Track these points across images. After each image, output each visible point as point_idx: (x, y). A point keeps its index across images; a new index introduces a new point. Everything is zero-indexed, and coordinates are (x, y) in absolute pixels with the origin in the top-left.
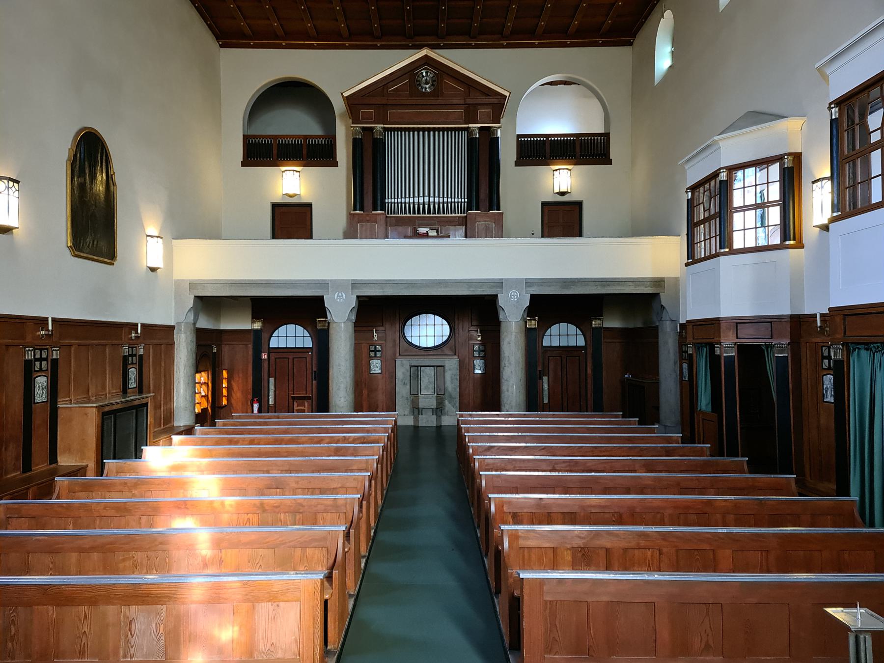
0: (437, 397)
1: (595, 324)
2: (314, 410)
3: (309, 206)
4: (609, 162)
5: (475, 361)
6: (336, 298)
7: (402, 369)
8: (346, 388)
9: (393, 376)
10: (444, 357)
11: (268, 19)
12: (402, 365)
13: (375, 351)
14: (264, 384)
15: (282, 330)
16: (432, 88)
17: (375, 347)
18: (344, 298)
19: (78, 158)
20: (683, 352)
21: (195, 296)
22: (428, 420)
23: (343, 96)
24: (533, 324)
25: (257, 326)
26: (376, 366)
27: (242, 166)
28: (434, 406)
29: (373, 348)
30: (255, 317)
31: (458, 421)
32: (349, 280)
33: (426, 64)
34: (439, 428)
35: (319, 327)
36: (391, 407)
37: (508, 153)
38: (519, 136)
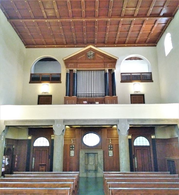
0: (95, 165)
1: (153, 137)
2: (49, 171)
4: (153, 81)
5: (109, 151)
6: (57, 126)
7: (82, 154)
8: (60, 162)
9: (78, 157)
10: (97, 149)
12: (82, 153)
13: (72, 147)
14: (31, 160)
15: (138, 138)
16: (93, 57)
17: (72, 146)
18: (60, 126)
20: (112, 147)
21: (6, 126)
22: (91, 175)
23: (63, 60)
24: (130, 137)
25: (30, 138)
26: (72, 153)
27: (121, 82)
28: (94, 169)
29: (71, 146)
30: (30, 134)
31: (104, 176)
32: (62, 119)
33: (91, 50)
34: (96, 178)
35: (52, 138)
36: (78, 170)
37: (118, 79)
38: (121, 73)
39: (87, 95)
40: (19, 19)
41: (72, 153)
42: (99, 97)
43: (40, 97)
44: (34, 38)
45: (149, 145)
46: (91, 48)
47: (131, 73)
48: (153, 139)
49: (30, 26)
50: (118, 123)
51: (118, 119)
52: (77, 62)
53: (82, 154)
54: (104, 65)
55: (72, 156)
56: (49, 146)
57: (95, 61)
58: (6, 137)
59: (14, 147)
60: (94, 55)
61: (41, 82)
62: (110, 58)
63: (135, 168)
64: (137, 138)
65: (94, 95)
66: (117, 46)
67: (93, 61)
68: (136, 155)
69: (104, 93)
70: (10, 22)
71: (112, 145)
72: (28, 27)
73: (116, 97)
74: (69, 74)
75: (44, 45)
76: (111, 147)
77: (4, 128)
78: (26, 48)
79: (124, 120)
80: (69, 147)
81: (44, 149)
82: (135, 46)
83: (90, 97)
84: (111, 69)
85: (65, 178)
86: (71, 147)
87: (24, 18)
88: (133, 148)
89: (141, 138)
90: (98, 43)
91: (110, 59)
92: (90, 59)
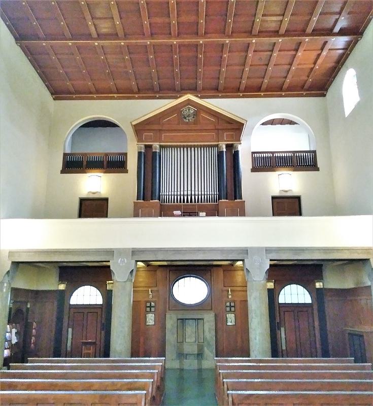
0: (198, 345)
1: (318, 285)
2: (101, 355)
3: (106, 200)
4: (318, 170)
5: (227, 315)
6: (119, 262)
7: (171, 321)
8: (124, 336)
9: (163, 327)
10: (203, 311)
11: (85, 80)
12: (171, 318)
13: (150, 307)
14: (64, 332)
16: (193, 119)
17: (151, 304)
18: (126, 262)
19: (255, 364)
20: (234, 307)
21: (12, 262)
22: (191, 364)
23: (132, 125)
24: (271, 285)
25: (62, 287)
26: (151, 319)
27: (252, 172)
28: (196, 352)
29: (148, 305)
30: (62, 279)
31: (216, 366)
32: (129, 249)
33: (189, 104)
34: (200, 370)
35: (109, 287)
36: (162, 353)
37: (245, 164)
38: (253, 153)
39: (182, 197)
40: (39, 39)
41: (151, 319)
42: (207, 202)
43: (83, 202)
44: (70, 80)
45: (310, 302)
46: (189, 100)
47: (273, 153)
48: (318, 289)
49: (63, 54)
50: (246, 255)
51: (246, 247)
52: (160, 130)
53: (171, 321)
54: (218, 135)
55: (150, 324)
56: (102, 303)
57: (198, 127)
58: (12, 286)
59: (29, 306)
60: (196, 114)
61: (86, 171)
62: (230, 121)
63: (282, 350)
64: (285, 288)
65: (195, 197)
66: (244, 97)
67: (193, 127)
68: (283, 323)
69: (218, 193)
70: (21, 46)
71: (234, 302)
72: (59, 57)
73: (241, 201)
74: (143, 154)
75: (91, 93)
76: (231, 306)
77: (8, 266)
78: (54, 99)
79: (259, 249)
80: (143, 306)
81: (92, 310)
82: (281, 96)
83: (187, 202)
84: (232, 144)
85: (136, 370)
86: (148, 307)
87: (49, 37)
88: (278, 309)
89: (294, 286)
90: (203, 89)
91: (229, 123)
92: (187, 123)
